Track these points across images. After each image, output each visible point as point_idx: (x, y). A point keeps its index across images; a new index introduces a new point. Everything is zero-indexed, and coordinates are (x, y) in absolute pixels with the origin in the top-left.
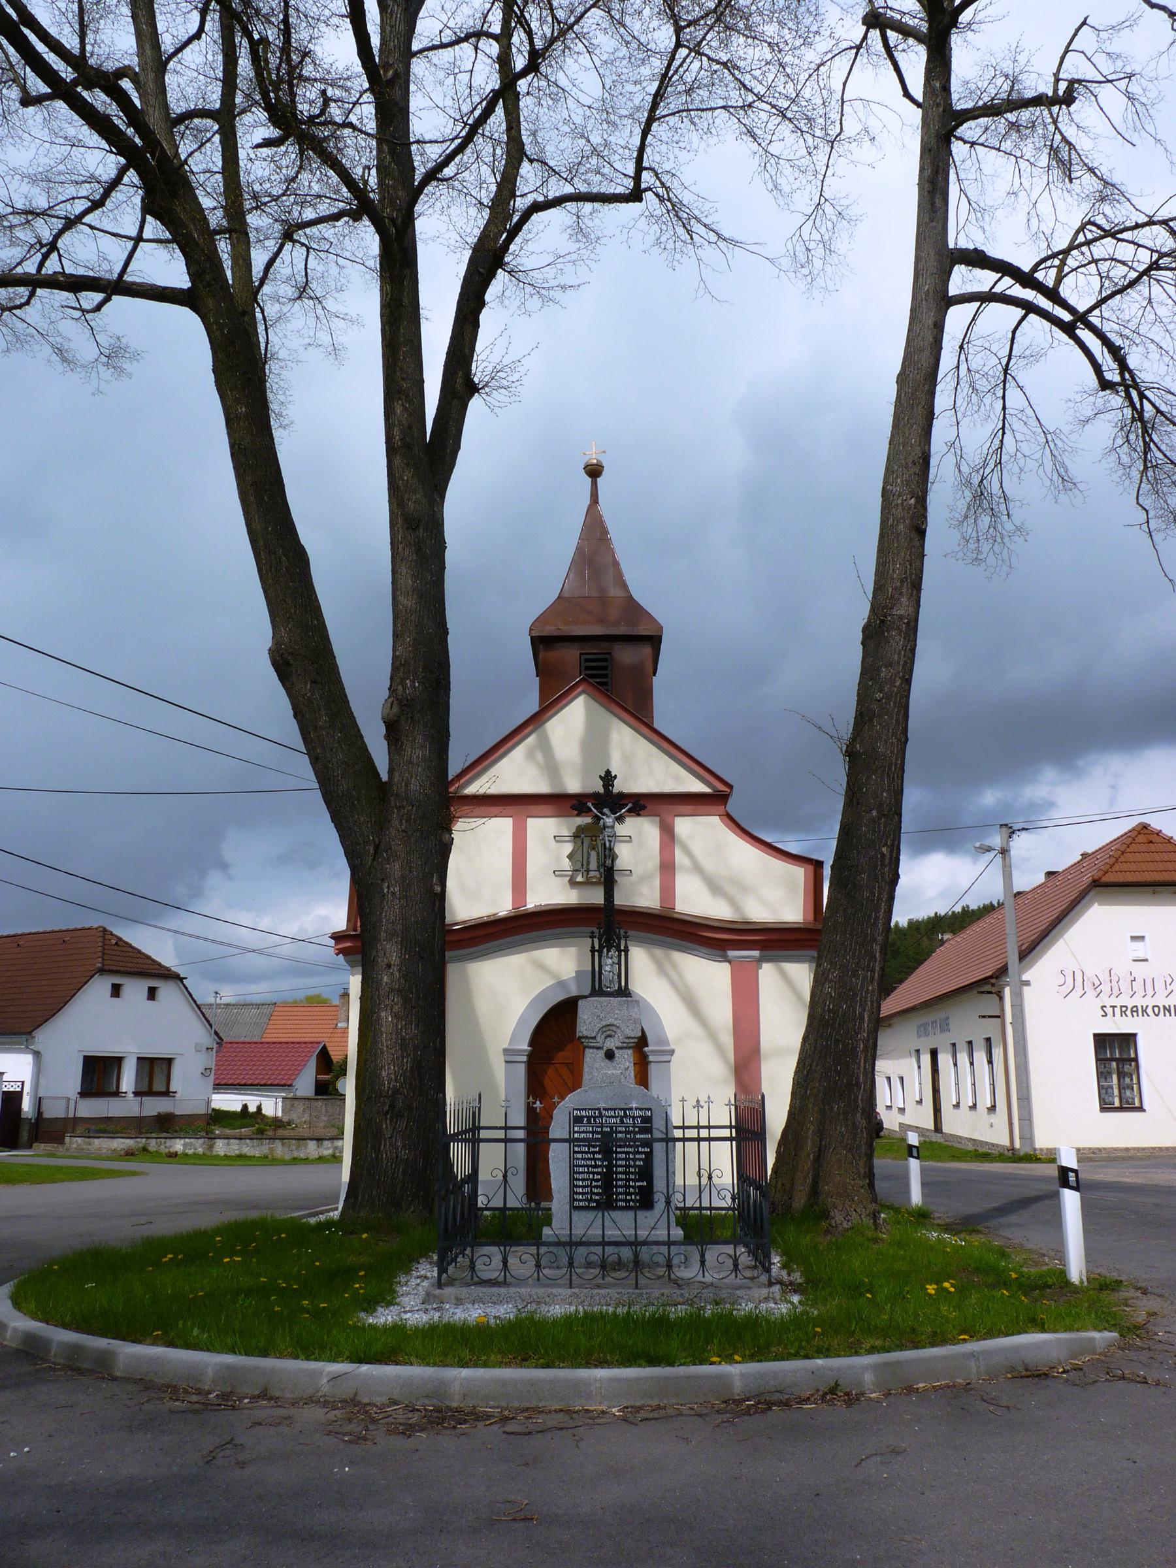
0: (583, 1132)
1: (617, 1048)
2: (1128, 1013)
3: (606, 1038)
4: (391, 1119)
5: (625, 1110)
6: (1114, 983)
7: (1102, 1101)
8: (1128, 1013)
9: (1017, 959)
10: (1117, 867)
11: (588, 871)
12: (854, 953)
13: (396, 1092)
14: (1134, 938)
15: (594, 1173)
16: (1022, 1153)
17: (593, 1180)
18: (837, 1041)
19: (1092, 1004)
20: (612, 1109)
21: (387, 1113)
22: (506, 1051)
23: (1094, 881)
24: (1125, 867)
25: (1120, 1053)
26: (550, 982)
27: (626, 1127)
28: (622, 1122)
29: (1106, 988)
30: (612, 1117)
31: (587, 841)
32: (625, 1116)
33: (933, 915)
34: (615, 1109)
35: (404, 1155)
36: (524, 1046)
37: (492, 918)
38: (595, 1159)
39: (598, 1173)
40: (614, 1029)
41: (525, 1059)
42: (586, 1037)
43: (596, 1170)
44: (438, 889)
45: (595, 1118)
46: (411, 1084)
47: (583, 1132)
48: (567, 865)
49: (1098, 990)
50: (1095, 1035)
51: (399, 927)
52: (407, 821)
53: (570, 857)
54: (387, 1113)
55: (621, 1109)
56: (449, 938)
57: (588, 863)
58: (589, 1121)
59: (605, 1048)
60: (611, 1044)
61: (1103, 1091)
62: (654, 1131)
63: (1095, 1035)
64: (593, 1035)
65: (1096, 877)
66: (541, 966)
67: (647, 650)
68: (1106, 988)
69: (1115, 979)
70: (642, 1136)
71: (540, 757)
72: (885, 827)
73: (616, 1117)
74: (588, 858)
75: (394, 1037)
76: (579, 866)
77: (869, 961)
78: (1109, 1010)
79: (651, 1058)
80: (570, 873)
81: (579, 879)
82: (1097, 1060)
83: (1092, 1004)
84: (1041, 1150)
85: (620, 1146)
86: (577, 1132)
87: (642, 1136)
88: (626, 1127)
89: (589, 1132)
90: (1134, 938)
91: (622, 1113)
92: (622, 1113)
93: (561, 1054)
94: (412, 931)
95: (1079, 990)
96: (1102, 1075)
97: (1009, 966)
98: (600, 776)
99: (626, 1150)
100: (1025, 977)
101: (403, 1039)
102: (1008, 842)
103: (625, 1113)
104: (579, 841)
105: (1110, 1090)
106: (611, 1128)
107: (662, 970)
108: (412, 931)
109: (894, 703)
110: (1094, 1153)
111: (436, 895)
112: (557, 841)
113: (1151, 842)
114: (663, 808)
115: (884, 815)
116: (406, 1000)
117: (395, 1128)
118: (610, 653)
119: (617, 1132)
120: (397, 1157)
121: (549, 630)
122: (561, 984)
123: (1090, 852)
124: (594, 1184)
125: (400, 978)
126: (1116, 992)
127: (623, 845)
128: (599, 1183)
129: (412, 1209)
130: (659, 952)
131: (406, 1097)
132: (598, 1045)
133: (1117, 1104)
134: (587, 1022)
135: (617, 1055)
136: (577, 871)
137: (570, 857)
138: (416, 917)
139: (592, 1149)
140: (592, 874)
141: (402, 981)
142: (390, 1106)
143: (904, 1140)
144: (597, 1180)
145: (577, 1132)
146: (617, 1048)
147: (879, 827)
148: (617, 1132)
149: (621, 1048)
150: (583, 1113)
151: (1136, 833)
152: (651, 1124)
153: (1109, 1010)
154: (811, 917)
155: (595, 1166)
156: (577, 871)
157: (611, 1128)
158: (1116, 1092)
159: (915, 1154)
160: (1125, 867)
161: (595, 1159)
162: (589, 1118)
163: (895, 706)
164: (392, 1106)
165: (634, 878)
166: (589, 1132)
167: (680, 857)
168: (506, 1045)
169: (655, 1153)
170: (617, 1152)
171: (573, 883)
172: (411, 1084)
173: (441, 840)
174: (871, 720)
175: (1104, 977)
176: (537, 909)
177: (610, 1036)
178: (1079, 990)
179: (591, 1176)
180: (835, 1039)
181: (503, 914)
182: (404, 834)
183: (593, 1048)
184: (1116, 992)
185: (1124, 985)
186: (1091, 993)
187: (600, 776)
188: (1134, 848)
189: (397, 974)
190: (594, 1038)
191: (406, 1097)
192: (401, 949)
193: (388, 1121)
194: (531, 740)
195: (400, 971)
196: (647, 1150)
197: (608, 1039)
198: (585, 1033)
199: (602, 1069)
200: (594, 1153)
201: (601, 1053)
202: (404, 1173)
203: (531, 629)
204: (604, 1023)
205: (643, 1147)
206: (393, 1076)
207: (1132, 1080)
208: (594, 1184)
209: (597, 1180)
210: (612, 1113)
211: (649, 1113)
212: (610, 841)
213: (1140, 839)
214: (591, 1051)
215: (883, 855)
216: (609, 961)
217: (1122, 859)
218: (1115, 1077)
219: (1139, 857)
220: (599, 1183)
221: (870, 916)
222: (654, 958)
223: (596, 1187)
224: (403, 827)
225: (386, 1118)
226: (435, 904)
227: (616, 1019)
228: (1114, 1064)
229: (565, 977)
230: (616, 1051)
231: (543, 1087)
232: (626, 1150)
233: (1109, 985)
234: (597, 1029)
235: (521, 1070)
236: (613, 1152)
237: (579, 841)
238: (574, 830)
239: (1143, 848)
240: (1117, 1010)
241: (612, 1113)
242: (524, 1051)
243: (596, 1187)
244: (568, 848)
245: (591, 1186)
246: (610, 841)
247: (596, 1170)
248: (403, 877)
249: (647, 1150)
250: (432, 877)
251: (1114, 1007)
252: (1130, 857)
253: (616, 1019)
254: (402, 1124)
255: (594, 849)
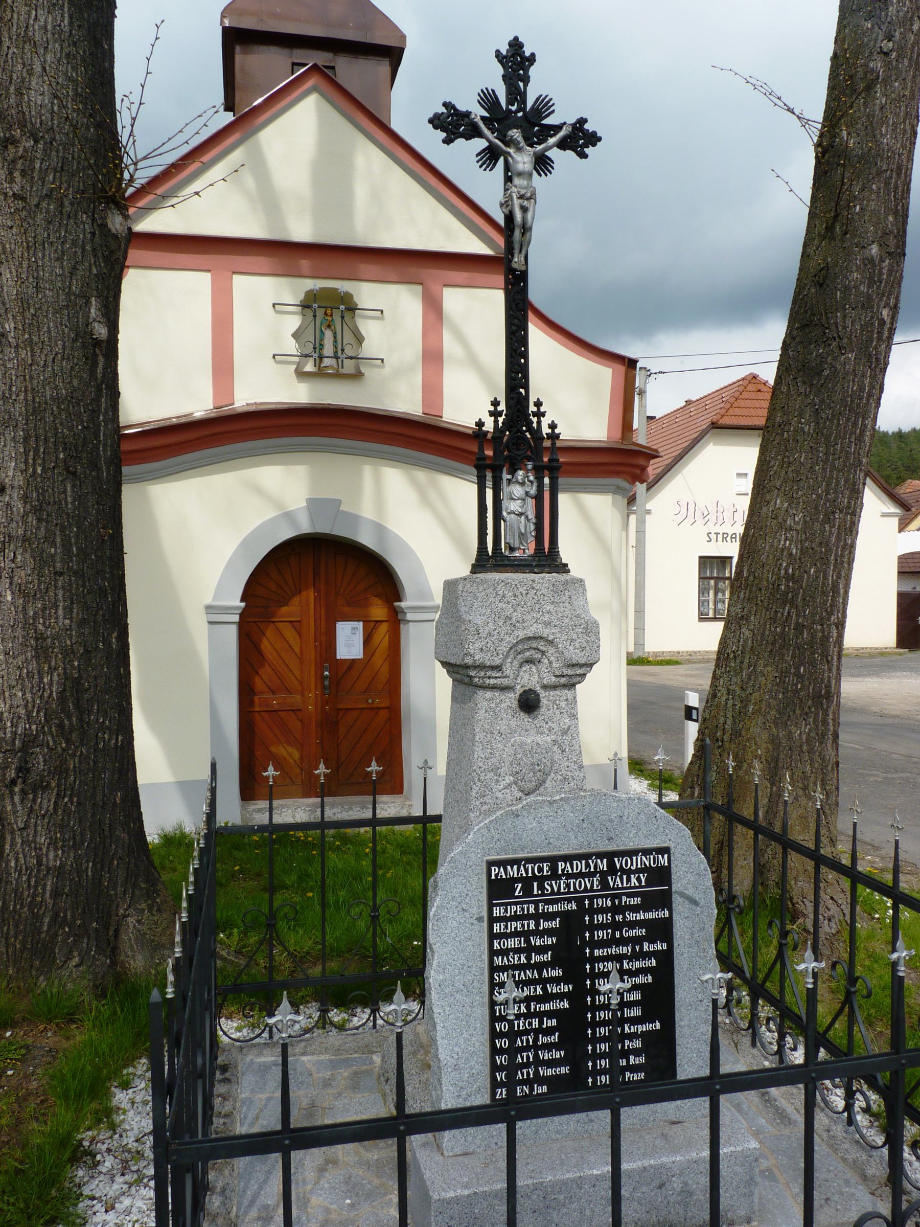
0: (516, 918)
1: (545, 687)
2: (729, 539)
3: (521, 666)
4: (24, 792)
5: (610, 856)
6: (720, 514)
7: (701, 613)
8: (729, 539)
9: (645, 491)
10: (731, 412)
11: (321, 357)
12: (828, 485)
13: (29, 742)
14: (739, 475)
15: (540, 1015)
16: (635, 657)
17: (537, 1032)
18: (799, 628)
19: (701, 530)
20: (579, 857)
21: (13, 782)
22: (209, 609)
23: (713, 423)
24: (738, 412)
25: (718, 573)
26: (271, 513)
27: (613, 897)
28: (604, 885)
29: (712, 517)
30: (581, 875)
31: (320, 313)
32: (612, 870)
33: (896, 430)
34: (586, 857)
35: (52, 858)
36: (235, 601)
37: (184, 420)
38: (543, 982)
39: (550, 1014)
40: (541, 645)
41: (236, 618)
42: (481, 667)
43: (547, 1007)
44: (101, 331)
45: (541, 880)
46: (61, 726)
47: (516, 918)
48: (291, 347)
49: (706, 519)
50: (700, 558)
51: (18, 409)
52: (23, 173)
53: (296, 335)
54: (13, 782)
55: (600, 855)
56: (125, 446)
57: (322, 345)
58: (527, 891)
59: (519, 690)
60: (529, 679)
61: (702, 603)
62: (677, 900)
63: (700, 558)
64: (497, 661)
65: (715, 420)
66: (258, 490)
67: (384, 68)
68: (712, 517)
69: (720, 509)
70: (650, 915)
71: (249, 180)
72: (889, 275)
73: (590, 875)
74: (322, 340)
75: (19, 632)
76: (309, 349)
77: (850, 498)
78: (713, 537)
79: (409, 616)
80: (297, 359)
81: (309, 367)
82: (700, 578)
83: (701, 530)
84: (649, 653)
85: (602, 944)
86: (500, 919)
87: (650, 915)
88: (613, 897)
89: (528, 917)
90: (739, 475)
91: (603, 865)
92: (603, 865)
93: (284, 609)
94: (49, 418)
95: (690, 519)
96: (702, 591)
97: (638, 496)
98: (498, 54)
99: (614, 950)
100: (648, 507)
101: (40, 637)
102: (645, 383)
103: (611, 865)
104: (310, 313)
105: (706, 604)
106: (579, 901)
107: (425, 500)
108: (49, 418)
109: (910, 60)
110: (690, 655)
111: (97, 343)
112: (277, 312)
113: (759, 391)
114: (431, 273)
115: (890, 254)
116: (42, 561)
117: (31, 810)
118: (333, 68)
119: (592, 911)
120: (39, 864)
121: (247, 23)
122: (288, 516)
123: (694, 399)
124: (543, 1040)
125: (26, 514)
126: (720, 521)
127: (370, 323)
128: (555, 1038)
129: (76, 960)
130: (421, 475)
131: (51, 749)
132: (505, 682)
133: (711, 615)
134: (484, 632)
135: (544, 702)
136: (306, 356)
137: (296, 335)
138: (56, 387)
139: (535, 958)
140: (327, 362)
141: (32, 519)
142: (19, 770)
143: (683, 698)
144: (549, 1031)
145: (500, 919)
146: (545, 687)
147: (881, 274)
148: (592, 911)
149: (554, 687)
150: (513, 872)
151: (746, 382)
152: (670, 885)
153: (713, 537)
154: (618, 435)
155: (546, 997)
156: (306, 356)
157: (579, 901)
158: (711, 606)
159: (695, 717)
160: (738, 412)
161: (543, 982)
162: (527, 882)
163: (910, 65)
164: (24, 770)
165: (387, 370)
166: (528, 917)
167: (449, 343)
168: (209, 601)
169: (676, 951)
170: (594, 960)
171: (301, 374)
172: (61, 726)
173: (104, 226)
174: (869, 88)
175: (712, 508)
176: (246, 409)
177: (529, 661)
178: (690, 519)
179: (535, 1023)
180: (797, 623)
181: (199, 414)
182: (21, 204)
183: (493, 688)
184: (720, 521)
185: (728, 515)
186: (700, 521)
187: (498, 54)
188: (745, 395)
189: (19, 506)
190: (498, 668)
191: (51, 749)
192: (26, 453)
193: (17, 799)
194: (237, 156)
195: (25, 499)
196: (660, 946)
197: (527, 667)
198: (479, 657)
199: (512, 732)
200: (540, 966)
201: (511, 699)
202: (56, 894)
203: (223, 16)
204: (521, 634)
205: (652, 941)
206: (22, 711)
207: (724, 595)
208: (543, 1040)
209: (549, 1031)
210: (580, 866)
211: (663, 860)
212: (524, 210)
213: (750, 388)
214: (489, 694)
215: (882, 322)
216: (518, 491)
217: (736, 404)
218: (712, 593)
219: (749, 403)
220: (555, 1038)
221: (855, 424)
222: (416, 484)
223: (548, 1047)
224: (16, 188)
225: (12, 794)
226: (95, 364)
227: (548, 624)
228: (712, 582)
229: (292, 507)
230: (543, 694)
231: (260, 652)
232: (614, 950)
233: (715, 514)
234: (504, 647)
235: (231, 635)
236: (586, 960)
237: (310, 313)
238: (302, 297)
239: (753, 395)
240: (720, 537)
241: (580, 866)
242: (236, 608)
243: (548, 1047)
244: (294, 322)
245: (536, 1047)
246: (524, 210)
247: (547, 1007)
248: (23, 302)
249: (660, 946)
250: (88, 303)
251: (717, 534)
252: (742, 403)
253: (548, 624)
254: (46, 802)
255: (329, 326)
